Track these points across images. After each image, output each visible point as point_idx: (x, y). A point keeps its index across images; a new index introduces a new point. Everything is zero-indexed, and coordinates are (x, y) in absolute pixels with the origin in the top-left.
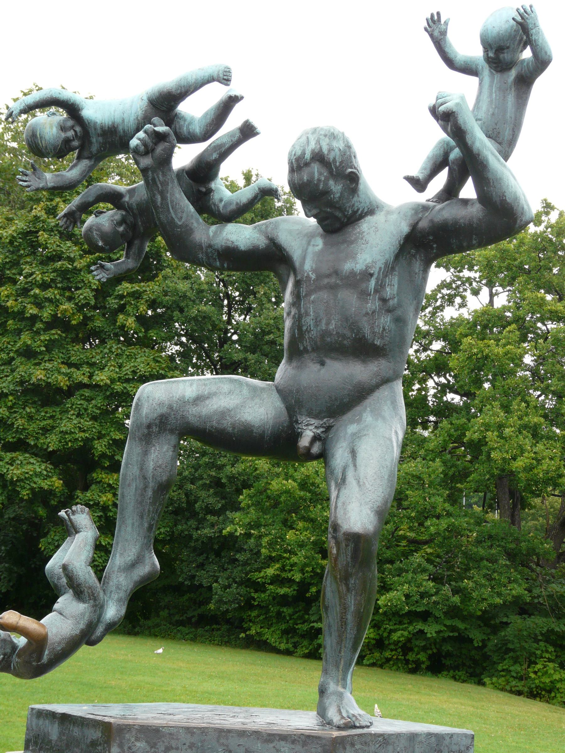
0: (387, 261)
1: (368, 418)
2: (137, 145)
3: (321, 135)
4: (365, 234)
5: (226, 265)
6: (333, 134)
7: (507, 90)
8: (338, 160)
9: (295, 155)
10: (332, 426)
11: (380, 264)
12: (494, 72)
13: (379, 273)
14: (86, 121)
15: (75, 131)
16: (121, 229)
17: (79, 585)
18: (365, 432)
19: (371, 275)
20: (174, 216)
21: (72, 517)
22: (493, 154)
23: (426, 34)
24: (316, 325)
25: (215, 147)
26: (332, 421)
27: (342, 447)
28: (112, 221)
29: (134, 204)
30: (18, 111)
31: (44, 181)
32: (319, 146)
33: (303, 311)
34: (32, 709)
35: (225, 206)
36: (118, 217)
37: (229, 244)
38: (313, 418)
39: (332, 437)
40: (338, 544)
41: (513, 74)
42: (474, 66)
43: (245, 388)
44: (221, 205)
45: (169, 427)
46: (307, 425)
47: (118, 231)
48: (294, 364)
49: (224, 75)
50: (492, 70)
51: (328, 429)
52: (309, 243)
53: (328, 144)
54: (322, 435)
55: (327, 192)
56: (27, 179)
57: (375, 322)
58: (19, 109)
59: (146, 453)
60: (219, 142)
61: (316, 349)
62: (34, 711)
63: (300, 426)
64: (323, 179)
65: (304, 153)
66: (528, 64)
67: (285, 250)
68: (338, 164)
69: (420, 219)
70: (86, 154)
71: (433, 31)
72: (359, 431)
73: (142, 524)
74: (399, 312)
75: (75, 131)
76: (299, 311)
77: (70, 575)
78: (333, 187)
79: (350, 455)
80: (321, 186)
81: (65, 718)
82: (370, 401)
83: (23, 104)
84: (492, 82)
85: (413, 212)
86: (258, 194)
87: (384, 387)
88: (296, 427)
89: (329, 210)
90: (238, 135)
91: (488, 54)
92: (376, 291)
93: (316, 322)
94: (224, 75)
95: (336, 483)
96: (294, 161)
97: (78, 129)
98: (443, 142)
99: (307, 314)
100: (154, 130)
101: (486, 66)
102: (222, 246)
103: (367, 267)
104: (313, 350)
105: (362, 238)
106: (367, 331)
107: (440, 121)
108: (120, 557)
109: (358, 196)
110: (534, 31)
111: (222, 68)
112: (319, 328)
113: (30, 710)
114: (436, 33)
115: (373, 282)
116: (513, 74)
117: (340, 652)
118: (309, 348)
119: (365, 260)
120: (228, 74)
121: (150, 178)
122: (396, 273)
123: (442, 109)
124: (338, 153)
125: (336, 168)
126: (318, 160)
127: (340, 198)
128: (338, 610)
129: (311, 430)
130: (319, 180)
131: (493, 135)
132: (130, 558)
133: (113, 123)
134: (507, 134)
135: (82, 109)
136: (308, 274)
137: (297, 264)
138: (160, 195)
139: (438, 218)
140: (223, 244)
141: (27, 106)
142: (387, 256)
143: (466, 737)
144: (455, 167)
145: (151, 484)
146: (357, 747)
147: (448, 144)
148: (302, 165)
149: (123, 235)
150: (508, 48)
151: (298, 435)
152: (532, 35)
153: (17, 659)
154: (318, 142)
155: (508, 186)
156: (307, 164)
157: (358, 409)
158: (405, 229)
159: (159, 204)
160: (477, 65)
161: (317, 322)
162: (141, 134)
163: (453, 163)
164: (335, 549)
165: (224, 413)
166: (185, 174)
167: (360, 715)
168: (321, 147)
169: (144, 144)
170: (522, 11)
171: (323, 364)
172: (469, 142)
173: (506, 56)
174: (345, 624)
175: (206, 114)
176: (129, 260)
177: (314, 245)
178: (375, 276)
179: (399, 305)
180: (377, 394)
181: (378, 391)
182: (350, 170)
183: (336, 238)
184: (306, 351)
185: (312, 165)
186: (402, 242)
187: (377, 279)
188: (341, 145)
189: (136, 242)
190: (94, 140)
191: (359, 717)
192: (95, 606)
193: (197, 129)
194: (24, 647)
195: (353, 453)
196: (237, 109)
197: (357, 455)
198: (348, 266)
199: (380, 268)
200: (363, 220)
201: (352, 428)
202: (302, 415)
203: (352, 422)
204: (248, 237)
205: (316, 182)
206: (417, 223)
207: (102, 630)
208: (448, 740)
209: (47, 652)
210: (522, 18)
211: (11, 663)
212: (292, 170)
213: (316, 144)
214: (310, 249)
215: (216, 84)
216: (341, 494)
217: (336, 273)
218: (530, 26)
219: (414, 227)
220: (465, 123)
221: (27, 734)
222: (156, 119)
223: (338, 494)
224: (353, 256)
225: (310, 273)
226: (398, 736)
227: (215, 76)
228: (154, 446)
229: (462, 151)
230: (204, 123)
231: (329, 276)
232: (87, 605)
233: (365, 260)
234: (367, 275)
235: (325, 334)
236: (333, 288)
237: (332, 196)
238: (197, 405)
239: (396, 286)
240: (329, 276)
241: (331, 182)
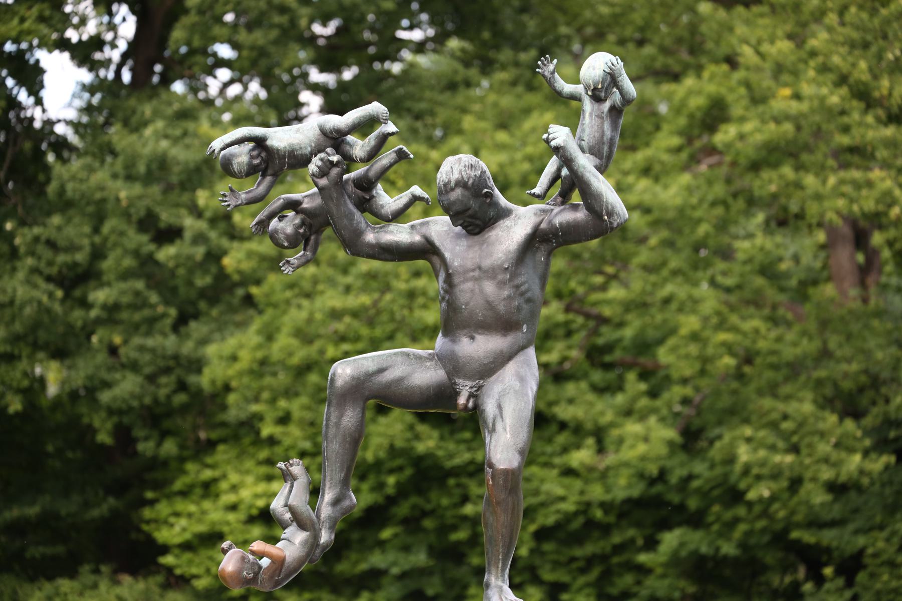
14: (271, 149)
15: (262, 157)
16: (302, 231)
21: (290, 469)
31: (240, 200)
36: (297, 221)
46: (463, 386)
47: (299, 232)
51: (480, 388)
56: (227, 200)
72: (504, 390)
79: (497, 410)
83: (223, 144)
87: (521, 353)
95: (488, 431)
97: (263, 155)
100: (329, 160)
110: (620, 78)
126: (461, 186)
135: (267, 139)
148: (449, 190)
149: (303, 235)
151: (457, 394)
163: (565, 178)
164: (491, 481)
165: (400, 380)
166: (350, 182)
170: (610, 64)
171: (472, 338)
182: (486, 190)
194: (268, 567)
197: (503, 409)
207: (319, 551)
216: (588, 96)
217: (480, 268)
222: (329, 150)
223: (548, 191)
231: (473, 270)
232: (308, 533)
236: (476, 279)
240: (473, 270)
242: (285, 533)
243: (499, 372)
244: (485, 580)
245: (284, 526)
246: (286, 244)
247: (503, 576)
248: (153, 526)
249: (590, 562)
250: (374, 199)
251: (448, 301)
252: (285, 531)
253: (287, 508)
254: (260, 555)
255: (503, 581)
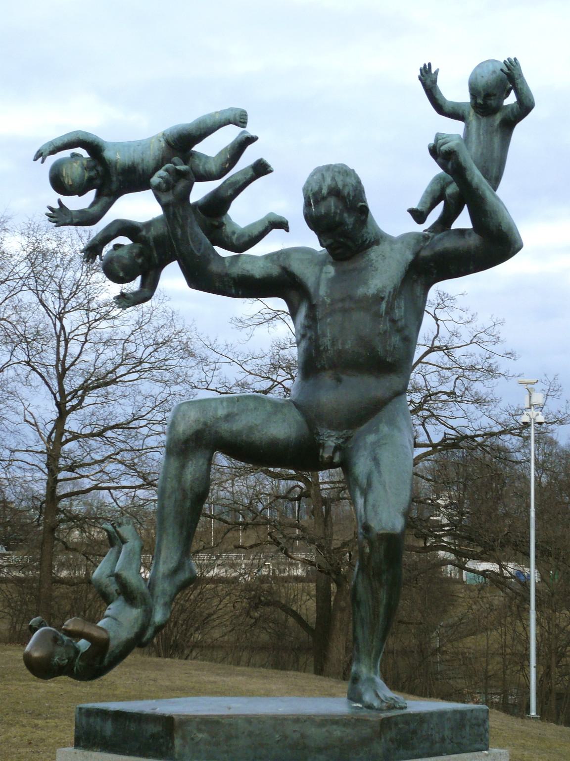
0: (395, 285)
1: (384, 429)
2: (160, 183)
3: (335, 172)
4: (374, 261)
5: (240, 293)
6: (346, 171)
7: (493, 132)
8: (352, 194)
9: (311, 191)
10: (352, 437)
11: (389, 289)
12: (480, 117)
13: (389, 297)
14: (107, 161)
15: (97, 171)
17: (132, 592)
18: (384, 442)
19: (383, 299)
20: (193, 248)
21: (118, 529)
22: (489, 189)
23: (419, 82)
24: (333, 345)
25: (230, 184)
26: (351, 432)
27: (363, 456)
28: (132, 253)
29: (151, 238)
30: (47, 152)
32: (334, 183)
33: (319, 332)
34: (81, 709)
35: (238, 239)
37: (245, 273)
38: (333, 430)
39: (352, 448)
40: (371, 544)
41: (498, 118)
42: (461, 112)
43: (268, 404)
44: (234, 238)
45: (204, 442)
46: (328, 437)
48: (311, 381)
49: (241, 118)
50: (478, 115)
51: (347, 439)
52: (321, 271)
53: (342, 180)
54: (342, 445)
55: (342, 223)
57: (387, 341)
58: (48, 150)
59: (183, 467)
60: (233, 180)
61: (333, 366)
62: (83, 710)
63: (321, 438)
64: (338, 211)
65: (321, 189)
66: (512, 109)
67: (298, 277)
68: (351, 198)
69: (422, 248)
70: (106, 191)
71: (426, 79)
72: (378, 441)
73: (181, 533)
74: (406, 333)
75: (97, 171)
76: (316, 333)
77: (124, 582)
78: (347, 220)
79: (373, 463)
80: (337, 219)
81: (119, 716)
82: (384, 413)
83: (52, 146)
84: (479, 124)
85: (415, 241)
86: (268, 227)
88: (317, 438)
89: (342, 240)
90: (251, 173)
91: (476, 101)
92: (387, 313)
93: (333, 342)
94: (241, 118)
96: (311, 195)
97: (100, 168)
98: (438, 179)
99: (324, 335)
100: (176, 169)
101: (472, 112)
102: (238, 275)
103: (379, 291)
104: (330, 368)
105: (371, 266)
106: (380, 350)
107: (439, 159)
108: (164, 564)
109: (367, 228)
110: (519, 81)
111: (238, 113)
112: (335, 348)
113: (78, 710)
114: (428, 82)
115: (384, 305)
116: (498, 118)
117: (372, 642)
118: (326, 366)
119: (376, 285)
120: (244, 117)
121: (171, 213)
122: (403, 297)
123: (444, 148)
124: (351, 189)
125: (350, 201)
126: (334, 195)
127: (352, 229)
128: (370, 604)
129: (332, 441)
130: (335, 213)
131: (486, 173)
132: (172, 565)
133: (133, 163)
134: (494, 171)
136: (324, 299)
137: (312, 290)
138: (181, 229)
139: (439, 248)
140: (240, 273)
141: (56, 147)
142: (396, 281)
143: (483, 711)
144: (452, 201)
145: (190, 495)
146: (401, 726)
147: (444, 179)
148: (319, 200)
150: (495, 95)
152: (517, 85)
153: (80, 663)
154: (333, 179)
155: (503, 217)
156: (324, 198)
157: (373, 421)
158: (410, 257)
159: (179, 237)
160: (463, 111)
161: (334, 342)
162: (162, 172)
166: (197, 209)
167: (396, 698)
168: (336, 183)
169: (167, 182)
172: (469, 178)
173: (492, 102)
174: (378, 617)
175: (220, 153)
176: (146, 290)
177: (326, 273)
178: (386, 300)
179: (406, 326)
180: (390, 407)
181: (390, 404)
182: (361, 204)
183: (347, 266)
184: (323, 369)
185: (329, 199)
186: (407, 268)
187: (388, 302)
188: (354, 182)
189: (151, 273)
190: (114, 179)
191: (396, 700)
192: (145, 611)
193: (213, 167)
195: (376, 460)
196: (250, 149)
198: (361, 291)
199: (390, 292)
200: (370, 249)
201: (371, 438)
202: (323, 427)
203: (370, 432)
204: (262, 266)
205: (332, 215)
206: (420, 251)
208: (468, 717)
209: (107, 655)
210: (509, 69)
211: (74, 666)
212: (307, 204)
213: (331, 180)
214: (323, 276)
215: (231, 126)
217: (351, 298)
218: (516, 76)
219: (417, 255)
220: (465, 160)
221: (76, 732)
222: (176, 159)
224: (365, 283)
225: (325, 298)
226: (431, 714)
227: (232, 119)
228: (192, 460)
229: (459, 186)
230: (219, 162)
231: (343, 300)
233: (376, 285)
234: (378, 299)
235: (340, 353)
237: (346, 227)
238: (228, 421)
239: (403, 308)
241: (346, 215)
242: (109, 609)
243: (371, 421)
244: (353, 671)
245: (107, 599)
246: (121, 274)
247: (375, 667)
248: (452, 350)
249: (229, 560)
250: (224, 227)
251: (310, 338)
252: (109, 607)
253: (113, 578)
254: (77, 635)
255: (376, 673)
